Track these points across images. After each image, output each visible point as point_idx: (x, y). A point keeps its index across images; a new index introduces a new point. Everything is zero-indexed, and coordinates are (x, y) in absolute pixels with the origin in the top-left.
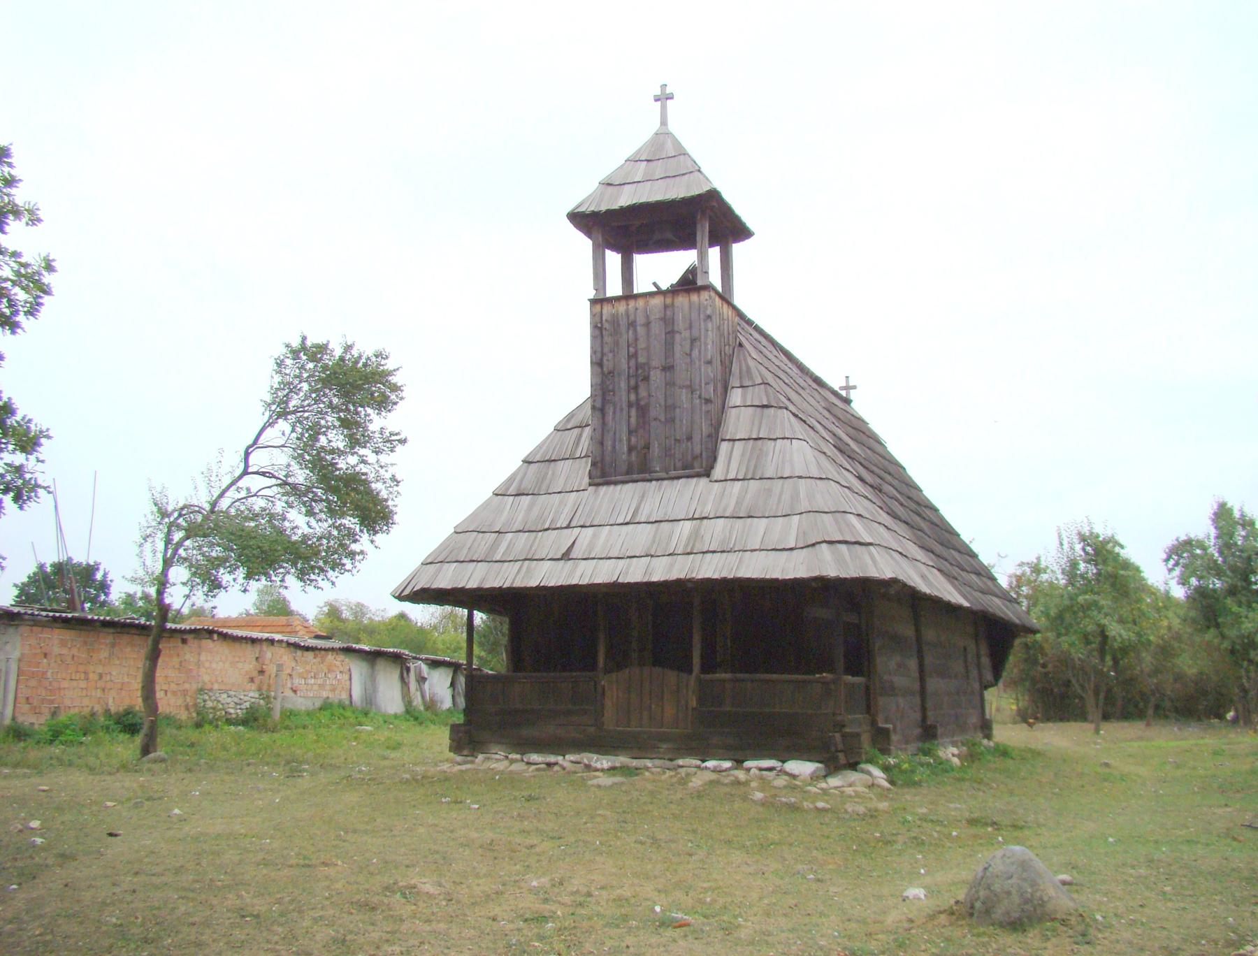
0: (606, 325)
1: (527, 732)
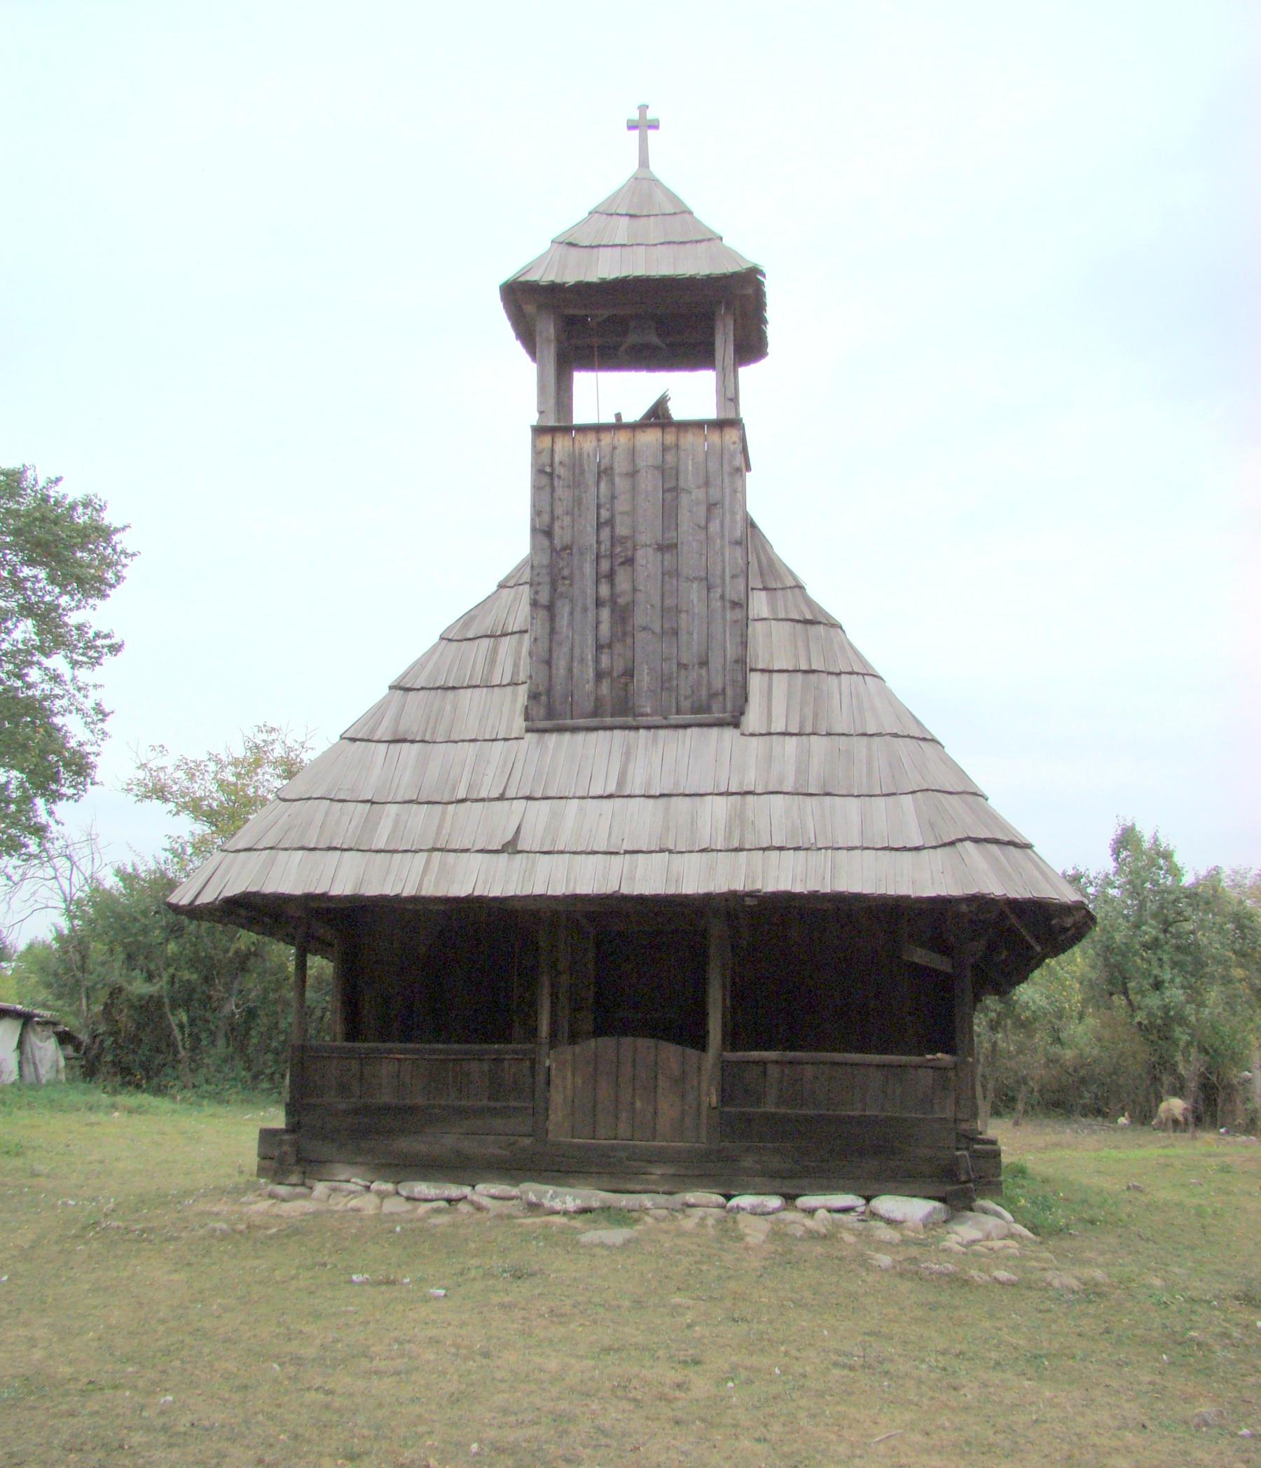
0: (560, 471)
1: (404, 1144)
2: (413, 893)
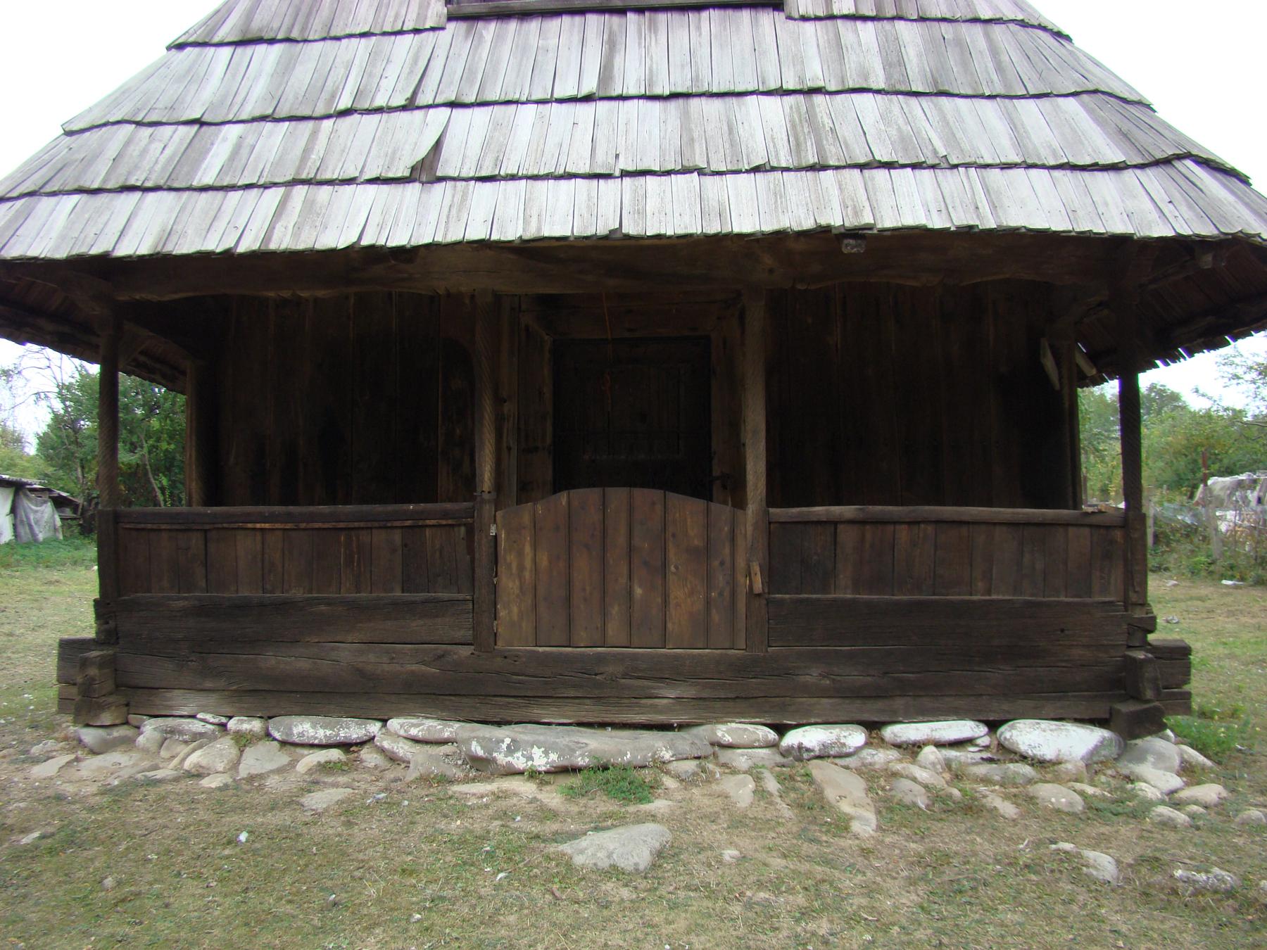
2: (255, 247)
